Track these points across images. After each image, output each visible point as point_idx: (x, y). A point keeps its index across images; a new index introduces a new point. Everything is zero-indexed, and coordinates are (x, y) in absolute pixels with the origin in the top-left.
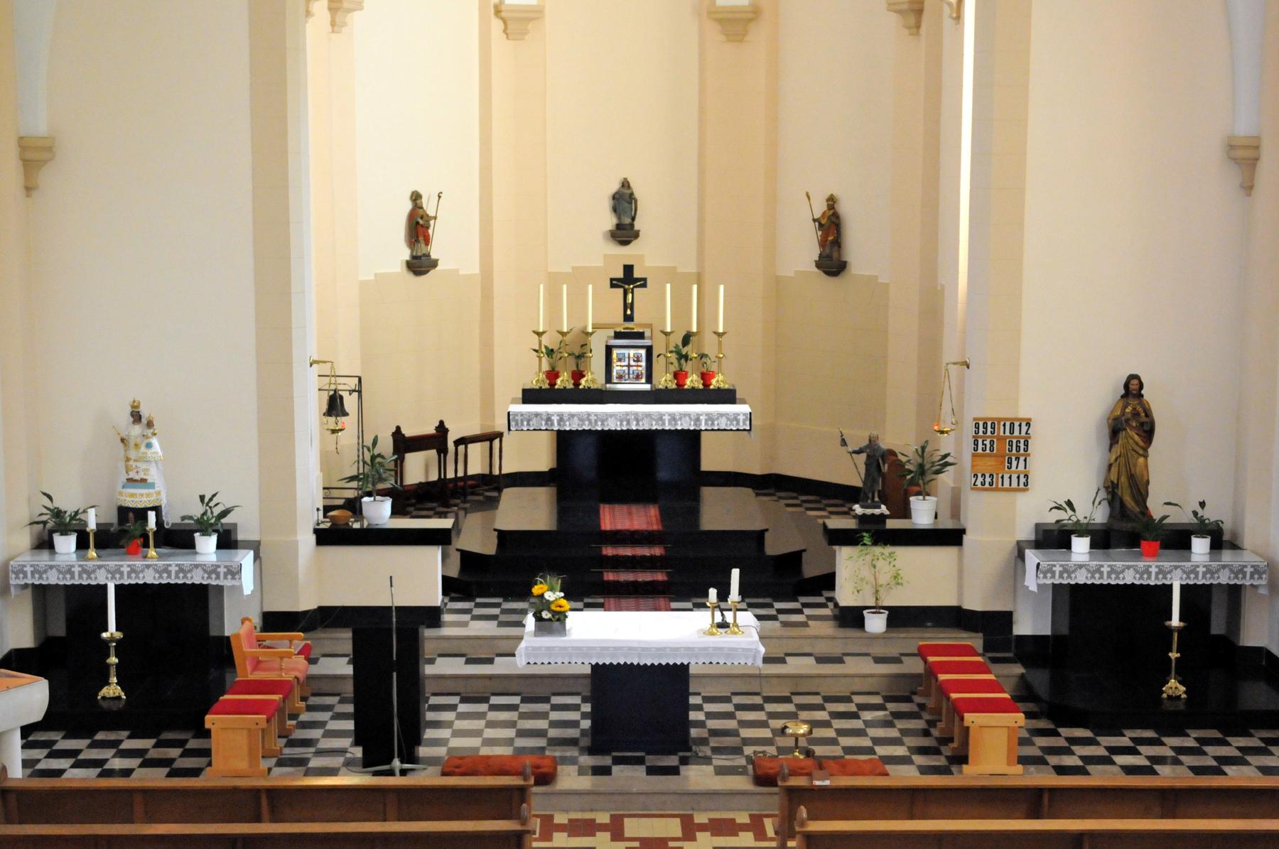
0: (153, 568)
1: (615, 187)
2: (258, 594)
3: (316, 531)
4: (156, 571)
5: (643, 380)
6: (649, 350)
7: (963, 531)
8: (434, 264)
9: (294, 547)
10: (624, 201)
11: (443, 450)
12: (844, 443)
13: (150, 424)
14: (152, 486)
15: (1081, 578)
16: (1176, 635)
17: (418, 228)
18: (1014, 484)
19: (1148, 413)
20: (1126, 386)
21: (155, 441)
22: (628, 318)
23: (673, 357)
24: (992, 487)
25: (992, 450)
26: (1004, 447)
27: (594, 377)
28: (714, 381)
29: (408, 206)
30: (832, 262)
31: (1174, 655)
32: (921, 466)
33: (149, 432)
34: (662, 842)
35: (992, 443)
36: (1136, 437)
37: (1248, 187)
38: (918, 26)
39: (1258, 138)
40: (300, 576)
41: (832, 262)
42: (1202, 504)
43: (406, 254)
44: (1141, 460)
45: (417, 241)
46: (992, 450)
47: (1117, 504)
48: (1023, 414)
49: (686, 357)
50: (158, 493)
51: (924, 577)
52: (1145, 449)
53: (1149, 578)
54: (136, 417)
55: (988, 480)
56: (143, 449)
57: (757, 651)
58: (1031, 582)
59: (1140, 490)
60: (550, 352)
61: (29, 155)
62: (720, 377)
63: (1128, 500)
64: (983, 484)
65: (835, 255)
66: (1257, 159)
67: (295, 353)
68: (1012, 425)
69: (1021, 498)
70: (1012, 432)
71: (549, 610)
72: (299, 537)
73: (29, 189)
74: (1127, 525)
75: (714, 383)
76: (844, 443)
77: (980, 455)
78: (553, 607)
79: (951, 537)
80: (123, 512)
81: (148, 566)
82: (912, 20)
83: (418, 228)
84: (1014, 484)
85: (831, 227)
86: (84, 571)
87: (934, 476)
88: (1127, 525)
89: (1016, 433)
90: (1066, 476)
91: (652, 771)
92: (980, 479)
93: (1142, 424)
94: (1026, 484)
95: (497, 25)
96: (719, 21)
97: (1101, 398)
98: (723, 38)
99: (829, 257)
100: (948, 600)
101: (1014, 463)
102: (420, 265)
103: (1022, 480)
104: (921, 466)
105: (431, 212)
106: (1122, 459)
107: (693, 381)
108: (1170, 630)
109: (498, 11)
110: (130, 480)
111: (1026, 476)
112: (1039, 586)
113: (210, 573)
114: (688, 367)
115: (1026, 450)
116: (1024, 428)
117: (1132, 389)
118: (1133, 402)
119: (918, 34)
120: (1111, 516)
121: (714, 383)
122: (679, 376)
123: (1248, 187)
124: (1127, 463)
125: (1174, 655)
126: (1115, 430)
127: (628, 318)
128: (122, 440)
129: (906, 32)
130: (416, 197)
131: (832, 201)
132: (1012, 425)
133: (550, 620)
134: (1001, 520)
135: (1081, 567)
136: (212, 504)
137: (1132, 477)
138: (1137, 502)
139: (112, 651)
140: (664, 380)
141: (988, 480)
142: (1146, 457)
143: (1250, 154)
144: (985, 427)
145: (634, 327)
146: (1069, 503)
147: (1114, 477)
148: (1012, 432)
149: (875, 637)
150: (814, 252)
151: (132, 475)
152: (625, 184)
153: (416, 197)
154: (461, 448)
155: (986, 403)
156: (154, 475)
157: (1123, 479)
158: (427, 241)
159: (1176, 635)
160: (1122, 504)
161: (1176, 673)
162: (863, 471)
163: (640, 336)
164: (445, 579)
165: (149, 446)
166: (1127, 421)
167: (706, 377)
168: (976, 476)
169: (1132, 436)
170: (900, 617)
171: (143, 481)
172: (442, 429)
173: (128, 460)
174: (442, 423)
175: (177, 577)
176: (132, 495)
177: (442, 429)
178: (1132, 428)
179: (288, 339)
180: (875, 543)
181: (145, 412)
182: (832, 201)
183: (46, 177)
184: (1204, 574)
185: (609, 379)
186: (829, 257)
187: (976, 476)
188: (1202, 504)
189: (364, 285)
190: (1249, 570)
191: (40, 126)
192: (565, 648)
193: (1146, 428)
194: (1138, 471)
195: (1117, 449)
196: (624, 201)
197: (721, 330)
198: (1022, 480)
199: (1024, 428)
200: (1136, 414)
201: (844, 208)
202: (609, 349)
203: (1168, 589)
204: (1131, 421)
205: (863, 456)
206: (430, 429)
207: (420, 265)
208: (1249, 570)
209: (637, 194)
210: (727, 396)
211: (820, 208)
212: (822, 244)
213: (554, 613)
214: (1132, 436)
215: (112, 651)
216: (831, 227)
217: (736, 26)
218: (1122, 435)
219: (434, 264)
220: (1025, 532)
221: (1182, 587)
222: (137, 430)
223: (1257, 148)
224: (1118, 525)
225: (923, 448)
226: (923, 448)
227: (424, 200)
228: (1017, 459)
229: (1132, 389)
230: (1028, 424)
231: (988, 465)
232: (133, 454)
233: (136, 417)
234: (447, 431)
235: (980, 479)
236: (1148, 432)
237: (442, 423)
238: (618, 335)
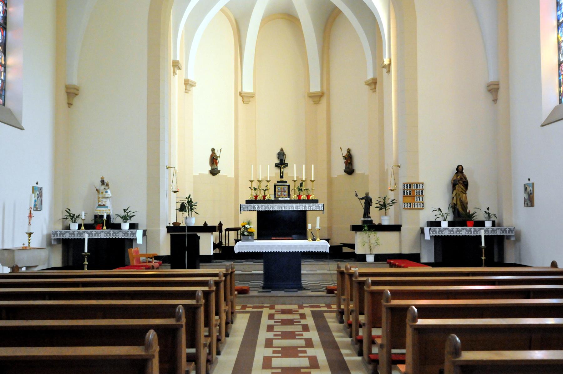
0: (104, 233)
1: (279, 151)
2: (145, 244)
3: (167, 227)
4: (105, 233)
5: (287, 196)
6: (289, 186)
7: (401, 226)
8: (219, 172)
9: (158, 232)
10: (281, 156)
11: (221, 231)
12: (357, 195)
13: (107, 185)
14: (107, 207)
15: (446, 233)
16: (483, 250)
17: (214, 160)
18: (419, 207)
19: (465, 178)
20: (457, 169)
21: (109, 191)
22: (282, 177)
23: (297, 190)
24: (411, 208)
25: (410, 194)
26: (414, 194)
27: (270, 196)
28: (311, 197)
29: (211, 153)
30: (350, 170)
31: (483, 258)
32: (384, 203)
33: (107, 188)
34: (297, 369)
35: (410, 192)
36: (462, 187)
37: (495, 100)
38: (375, 88)
39: (498, 84)
40: (161, 243)
41: (350, 170)
42: (488, 209)
43: (210, 168)
44: (464, 195)
45: (213, 164)
46: (410, 194)
47: (457, 211)
48: (420, 181)
49: (301, 190)
50: (110, 210)
51: (388, 243)
52: (466, 192)
53: (471, 233)
54: (103, 182)
55: (409, 205)
56: (104, 193)
57: (327, 246)
58: (427, 237)
59: (464, 206)
60: (255, 189)
61: (69, 91)
62: (313, 196)
63: (460, 209)
64: (407, 207)
65: (350, 167)
66: (498, 89)
67: (161, 164)
68: (417, 185)
69: (421, 212)
70: (417, 188)
71: (247, 232)
72: (161, 228)
73: (70, 104)
74: (461, 216)
75: (311, 198)
76: (357, 195)
77: (406, 196)
78: (249, 230)
79: (396, 228)
80: (96, 216)
81: (102, 232)
82: (373, 87)
83: (214, 160)
84: (419, 207)
85: (349, 159)
86: (79, 233)
87: (389, 207)
88: (461, 216)
89: (419, 188)
90: (437, 202)
91: (285, 292)
92: (406, 205)
93: (464, 182)
94: (423, 207)
95: (240, 99)
96: (310, 97)
97: (449, 174)
98: (312, 103)
99: (348, 168)
100: (396, 251)
101: (418, 199)
102: (214, 172)
103: (421, 205)
104: (384, 203)
105: (218, 155)
106: (457, 195)
107: (304, 197)
108: (482, 248)
109: (240, 94)
110: (99, 205)
111: (423, 204)
112: (431, 236)
113: (125, 234)
114: (302, 193)
115: (422, 194)
116: (421, 186)
117: (460, 170)
118: (460, 175)
119: (375, 91)
120: (454, 217)
121: (311, 198)
122: (299, 196)
123: (495, 100)
124: (459, 196)
125: (483, 258)
126: (454, 184)
127: (282, 177)
128: (97, 190)
129: (371, 91)
130: (213, 150)
131: (349, 151)
132: (417, 185)
133: (247, 235)
134: (414, 221)
135: (446, 229)
136: (127, 211)
137: (461, 201)
138: (463, 210)
139: (86, 259)
140: (294, 196)
141: (409, 205)
142: (466, 194)
143: (496, 87)
144: (407, 186)
145: (284, 179)
146: (439, 209)
147: (454, 202)
148: (417, 188)
149: (371, 263)
150: (344, 167)
151: (100, 203)
152: (282, 150)
153: (213, 150)
154: (227, 232)
155: (406, 178)
156: (108, 203)
157: (458, 202)
158: (217, 164)
159: (483, 250)
160: (458, 211)
161: (457, 357)
162: (364, 205)
163: (286, 182)
164: (214, 244)
165: (106, 192)
166: (458, 181)
167: (308, 196)
168: (405, 204)
169: (460, 187)
170: (379, 258)
171: (104, 205)
172: (221, 225)
173: (99, 198)
174: (220, 222)
175: (113, 235)
176: (100, 211)
177: (221, 225)
178: (460, 183)
179: (158, 159)
180: (369, 230)
181: (106, 181)
182: (349, 151)
183: (76, 101)
184: (491, 231)
185: (275, 197)
186: (348, 168)
187: (405, 204)
188: (488, 209)
189: (195, 177)
190: (508, 230)
191: (74, 81)
192: (253, 246)
193: (466, 183)
194: (463, 199)
195: (455, 192)
196: (281, 156)
197: (313, 179)
198: (421, 205)
199: (421, 186)
200: (461, 179)
201: (353, 153)
202: (275, 186)
203: (480, 236)
204: (460, 181)
205: (364, 200)
206: (216, 224)
207: (214, 172)
208: (508, 230)
209: (285, 153)
210: (316, 201)
211: (345, 153)
212: (346, 164)
213: (250, 232)
214: (460, 187)
215: (86, 259)
216: (349, 159)
217: (317, 98)
218: (457, 186)
219: (219, 172)
220: (423, 224)
221: (485, 236)
222: (103, 187)
223: (498, 84)
224: (457, 219)
225: (385, 198)
226: (385, 198)
227: (216, 151)
228: (419, 197)
229: (460, 170)
230: (423, 185)
231: (409, 200)
232: (101, 196)
233: (103, 182)
234: (222, 225)
235: (406, 205)
236: (466, 185)
237: (220, 222)
238: (278, 182)
